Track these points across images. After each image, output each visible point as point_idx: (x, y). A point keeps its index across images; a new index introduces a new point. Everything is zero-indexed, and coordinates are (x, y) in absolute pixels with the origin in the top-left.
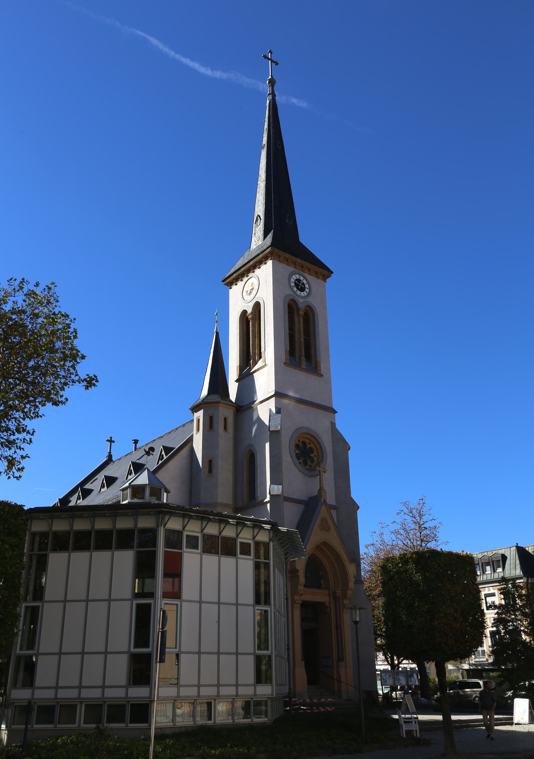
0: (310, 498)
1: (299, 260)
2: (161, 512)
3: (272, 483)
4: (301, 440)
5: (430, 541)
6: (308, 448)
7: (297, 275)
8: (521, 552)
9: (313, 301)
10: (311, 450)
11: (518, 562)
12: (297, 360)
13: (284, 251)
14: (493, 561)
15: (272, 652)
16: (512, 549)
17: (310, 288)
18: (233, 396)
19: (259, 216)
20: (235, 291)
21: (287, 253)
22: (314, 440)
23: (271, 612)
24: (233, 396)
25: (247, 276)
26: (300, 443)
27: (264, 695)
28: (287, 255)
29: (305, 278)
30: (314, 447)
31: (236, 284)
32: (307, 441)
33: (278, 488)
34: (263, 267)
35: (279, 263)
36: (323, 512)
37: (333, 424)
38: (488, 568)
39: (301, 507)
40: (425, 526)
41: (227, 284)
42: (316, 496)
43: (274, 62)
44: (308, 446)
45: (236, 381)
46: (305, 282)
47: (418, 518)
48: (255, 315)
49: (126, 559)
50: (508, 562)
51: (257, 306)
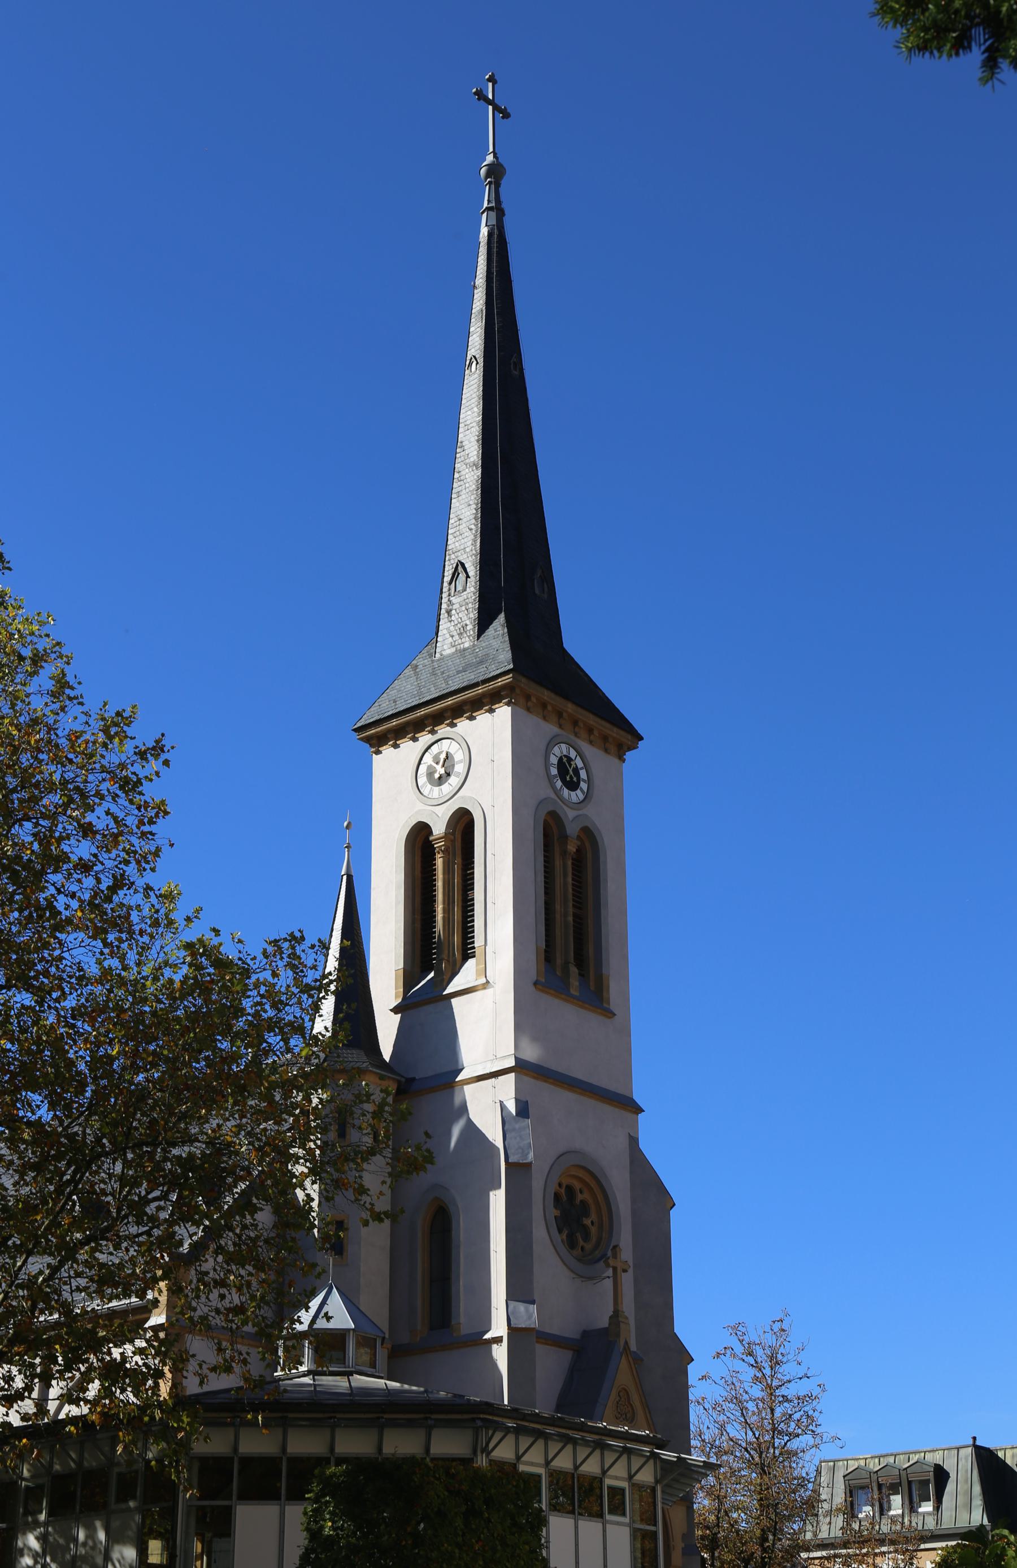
0: (586, 1334)
1: (570, 708)
2: (488, 1424)
3: (512, 1295)
4: (565, 1182)
5: (798, 1436)
6: (578, 1202)
7: (563, 746)
8: (987, 1461)
9: (597, 816)
10: (584, 1209)
11: (977, 1489)
12: (559, 973)
13: (540, 683)
14: (910, 1483)
16: (962, 1452)
17: (589, 781)
18: (387, 1050)
19: (463, 565)
20: (394, 767)
21: (548, 688)
22: (593, 1184)
24: (387, 1050)
25: (433, 732)
26: (563, 1191)
28: (546, 695)
29: (579, 753)
30: (590, 1201)
31: (396, 746)
32: (577, 1185)
33: (527, 1310)
34: (483, 718)
35: (525, 712)
36: (622, 1375)
37: (633, 1141)
38: (896, 1500)
39: (565, 1357)
40: (783, 1391)
41: (368, 740)
42: (605, 1331)
43: (501, 111)
44: (580, 1197)
45: (395, 1010)
46: (579, 763)
47: (767, 1371)
48: (453, 841)
50: (950, 1487)
51: (463, 824)
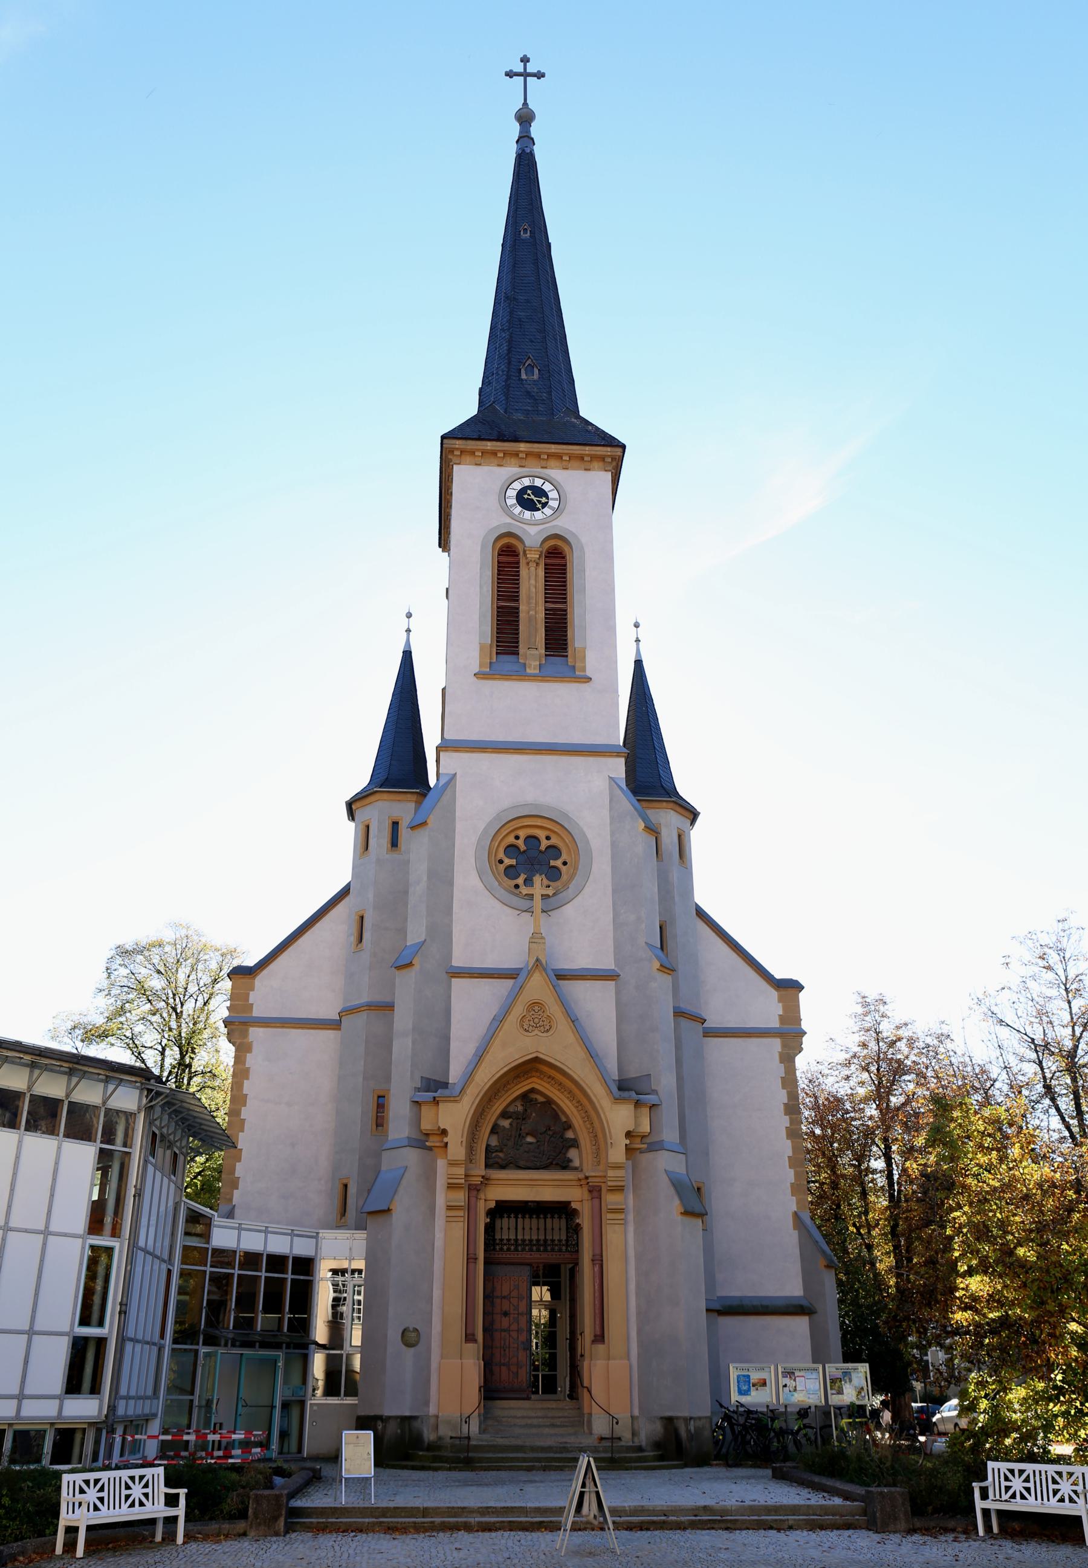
1: (523, 447)
15: (110, 1331)
23: (121, 1251)
27: (80, 1417)
49: (81, 1156)
